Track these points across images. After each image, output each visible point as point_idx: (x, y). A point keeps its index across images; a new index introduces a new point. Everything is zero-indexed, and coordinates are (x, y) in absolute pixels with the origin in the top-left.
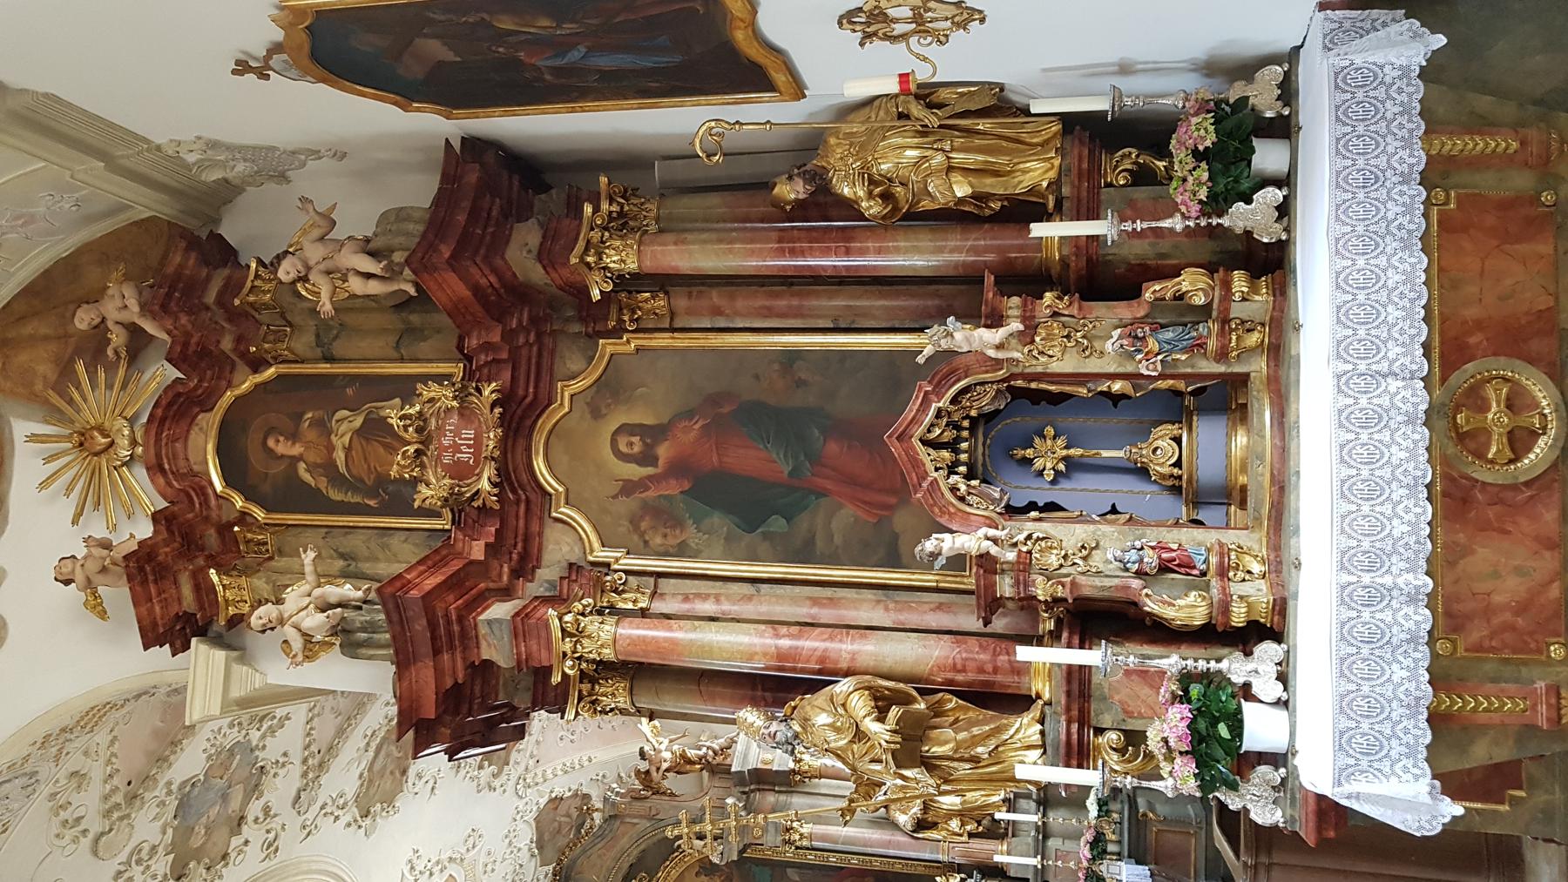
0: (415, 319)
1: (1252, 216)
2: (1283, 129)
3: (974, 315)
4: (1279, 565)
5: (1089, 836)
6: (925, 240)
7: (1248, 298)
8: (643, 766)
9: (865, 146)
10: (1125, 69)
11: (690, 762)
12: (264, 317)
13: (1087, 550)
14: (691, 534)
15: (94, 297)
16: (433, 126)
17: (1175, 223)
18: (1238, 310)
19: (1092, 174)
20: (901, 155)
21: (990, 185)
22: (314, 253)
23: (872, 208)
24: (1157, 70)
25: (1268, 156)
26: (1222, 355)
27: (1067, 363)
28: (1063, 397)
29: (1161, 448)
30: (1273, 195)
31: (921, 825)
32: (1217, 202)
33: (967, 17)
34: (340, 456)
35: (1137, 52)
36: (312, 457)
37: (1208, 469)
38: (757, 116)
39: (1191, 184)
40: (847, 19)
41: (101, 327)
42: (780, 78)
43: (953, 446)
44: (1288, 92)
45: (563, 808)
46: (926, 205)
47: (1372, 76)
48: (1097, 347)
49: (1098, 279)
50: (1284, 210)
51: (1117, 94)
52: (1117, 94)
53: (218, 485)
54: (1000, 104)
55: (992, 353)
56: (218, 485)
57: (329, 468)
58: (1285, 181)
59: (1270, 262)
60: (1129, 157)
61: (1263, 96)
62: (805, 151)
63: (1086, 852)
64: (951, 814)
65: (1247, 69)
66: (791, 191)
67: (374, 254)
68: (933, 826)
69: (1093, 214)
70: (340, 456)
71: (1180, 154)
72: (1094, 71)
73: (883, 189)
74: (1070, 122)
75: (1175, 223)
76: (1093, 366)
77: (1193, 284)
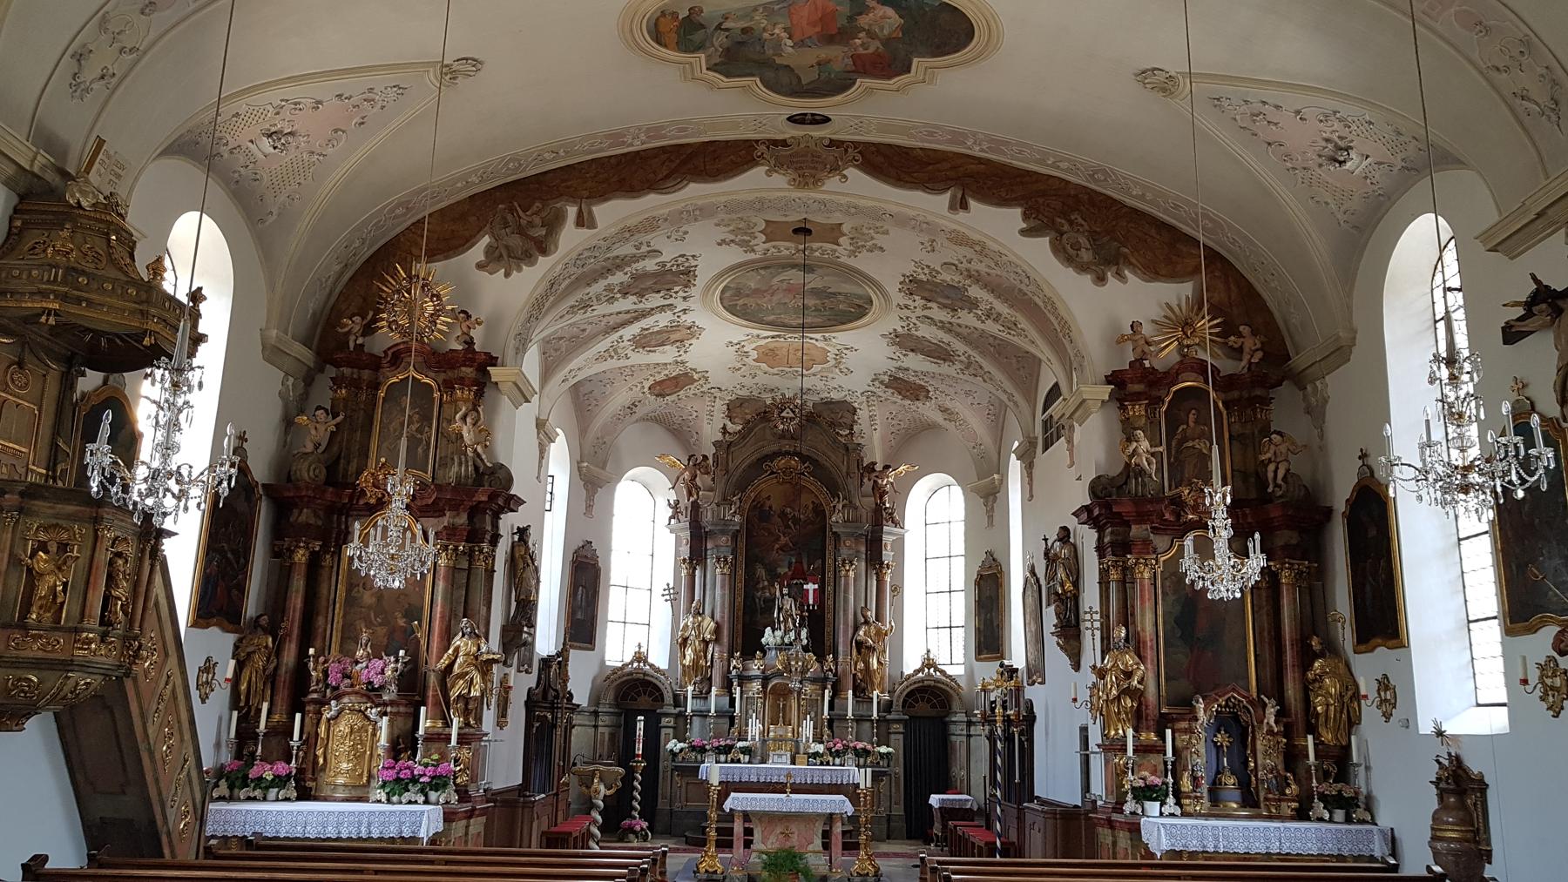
0: (1253, 480)
1: (1319, 808)
2: (1349, 820)
3: (1278, 715)
4: (1199, 815)
5: (869, 747)
6: (1300, 696)
7: (1288, 808)
8: (879, 467)
9: (1334, 674)
10: (1368, 768)
11: (881, 498)
12: (1249, 411)
13: (1197, 753)
14: (1171, 598)
15: (1254, 333)
16: (1340, 506)
17: (1315, 784)
18: (1284, 804)
19: (1327, 757)
20: (1332, 686)
21: (1322, 720)
22: (1283, 448)
23: (1310, 675)
24: (1367, 779)
25: (1339, 814)
26: (1266, 799)
27: (1259, 746)
28: (1245, 747)
29: (1230, 781)
30: (1327, 816)
31: (860, 645)
32: (1322, 797)
33: (950, 34)
34: (1190, 444)
35: (1374, 773)
36: (1189, 432)
37: (1224, 794)
38: (1346, 636)
39: (1331, 789)
40: (1385, 677)
41: (1240, 335)
42: (1362, 648)
43: (1227, 705)
44: (1363, 822)
45: (848, 415)
46: (1312, 695)
47: (1371, 842)
48: (1265, 758)
49: (1292, 757)
50: (1321, 820)
51: (1358, 765)
52: (1358, 765)
53: (1174, 389)
54: (1353, 722)
55: (509, 522)
56: (1174, 389)
57: (1185, 439)
58: (1331, 821)
59: (1302, 815)
60: (1334, 770)
61: (1360, 813)
62: (1331, 649)
63: (860, 745)
64: (867, 664)
65: (1369, 809)
66: (1315, 643)
67: (1285, 479)
68: (859, 652)
69: (1135, 751)
70: (1190, 444)
71: (1339, 785)
72: (1367, 758)
73: (1319, 679)
74: (1347, 748)
75: (1315, 784)
76: (1260, 756)
77: (1292, 790)
